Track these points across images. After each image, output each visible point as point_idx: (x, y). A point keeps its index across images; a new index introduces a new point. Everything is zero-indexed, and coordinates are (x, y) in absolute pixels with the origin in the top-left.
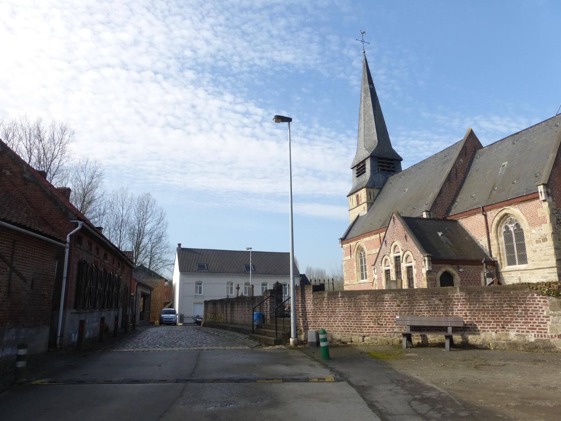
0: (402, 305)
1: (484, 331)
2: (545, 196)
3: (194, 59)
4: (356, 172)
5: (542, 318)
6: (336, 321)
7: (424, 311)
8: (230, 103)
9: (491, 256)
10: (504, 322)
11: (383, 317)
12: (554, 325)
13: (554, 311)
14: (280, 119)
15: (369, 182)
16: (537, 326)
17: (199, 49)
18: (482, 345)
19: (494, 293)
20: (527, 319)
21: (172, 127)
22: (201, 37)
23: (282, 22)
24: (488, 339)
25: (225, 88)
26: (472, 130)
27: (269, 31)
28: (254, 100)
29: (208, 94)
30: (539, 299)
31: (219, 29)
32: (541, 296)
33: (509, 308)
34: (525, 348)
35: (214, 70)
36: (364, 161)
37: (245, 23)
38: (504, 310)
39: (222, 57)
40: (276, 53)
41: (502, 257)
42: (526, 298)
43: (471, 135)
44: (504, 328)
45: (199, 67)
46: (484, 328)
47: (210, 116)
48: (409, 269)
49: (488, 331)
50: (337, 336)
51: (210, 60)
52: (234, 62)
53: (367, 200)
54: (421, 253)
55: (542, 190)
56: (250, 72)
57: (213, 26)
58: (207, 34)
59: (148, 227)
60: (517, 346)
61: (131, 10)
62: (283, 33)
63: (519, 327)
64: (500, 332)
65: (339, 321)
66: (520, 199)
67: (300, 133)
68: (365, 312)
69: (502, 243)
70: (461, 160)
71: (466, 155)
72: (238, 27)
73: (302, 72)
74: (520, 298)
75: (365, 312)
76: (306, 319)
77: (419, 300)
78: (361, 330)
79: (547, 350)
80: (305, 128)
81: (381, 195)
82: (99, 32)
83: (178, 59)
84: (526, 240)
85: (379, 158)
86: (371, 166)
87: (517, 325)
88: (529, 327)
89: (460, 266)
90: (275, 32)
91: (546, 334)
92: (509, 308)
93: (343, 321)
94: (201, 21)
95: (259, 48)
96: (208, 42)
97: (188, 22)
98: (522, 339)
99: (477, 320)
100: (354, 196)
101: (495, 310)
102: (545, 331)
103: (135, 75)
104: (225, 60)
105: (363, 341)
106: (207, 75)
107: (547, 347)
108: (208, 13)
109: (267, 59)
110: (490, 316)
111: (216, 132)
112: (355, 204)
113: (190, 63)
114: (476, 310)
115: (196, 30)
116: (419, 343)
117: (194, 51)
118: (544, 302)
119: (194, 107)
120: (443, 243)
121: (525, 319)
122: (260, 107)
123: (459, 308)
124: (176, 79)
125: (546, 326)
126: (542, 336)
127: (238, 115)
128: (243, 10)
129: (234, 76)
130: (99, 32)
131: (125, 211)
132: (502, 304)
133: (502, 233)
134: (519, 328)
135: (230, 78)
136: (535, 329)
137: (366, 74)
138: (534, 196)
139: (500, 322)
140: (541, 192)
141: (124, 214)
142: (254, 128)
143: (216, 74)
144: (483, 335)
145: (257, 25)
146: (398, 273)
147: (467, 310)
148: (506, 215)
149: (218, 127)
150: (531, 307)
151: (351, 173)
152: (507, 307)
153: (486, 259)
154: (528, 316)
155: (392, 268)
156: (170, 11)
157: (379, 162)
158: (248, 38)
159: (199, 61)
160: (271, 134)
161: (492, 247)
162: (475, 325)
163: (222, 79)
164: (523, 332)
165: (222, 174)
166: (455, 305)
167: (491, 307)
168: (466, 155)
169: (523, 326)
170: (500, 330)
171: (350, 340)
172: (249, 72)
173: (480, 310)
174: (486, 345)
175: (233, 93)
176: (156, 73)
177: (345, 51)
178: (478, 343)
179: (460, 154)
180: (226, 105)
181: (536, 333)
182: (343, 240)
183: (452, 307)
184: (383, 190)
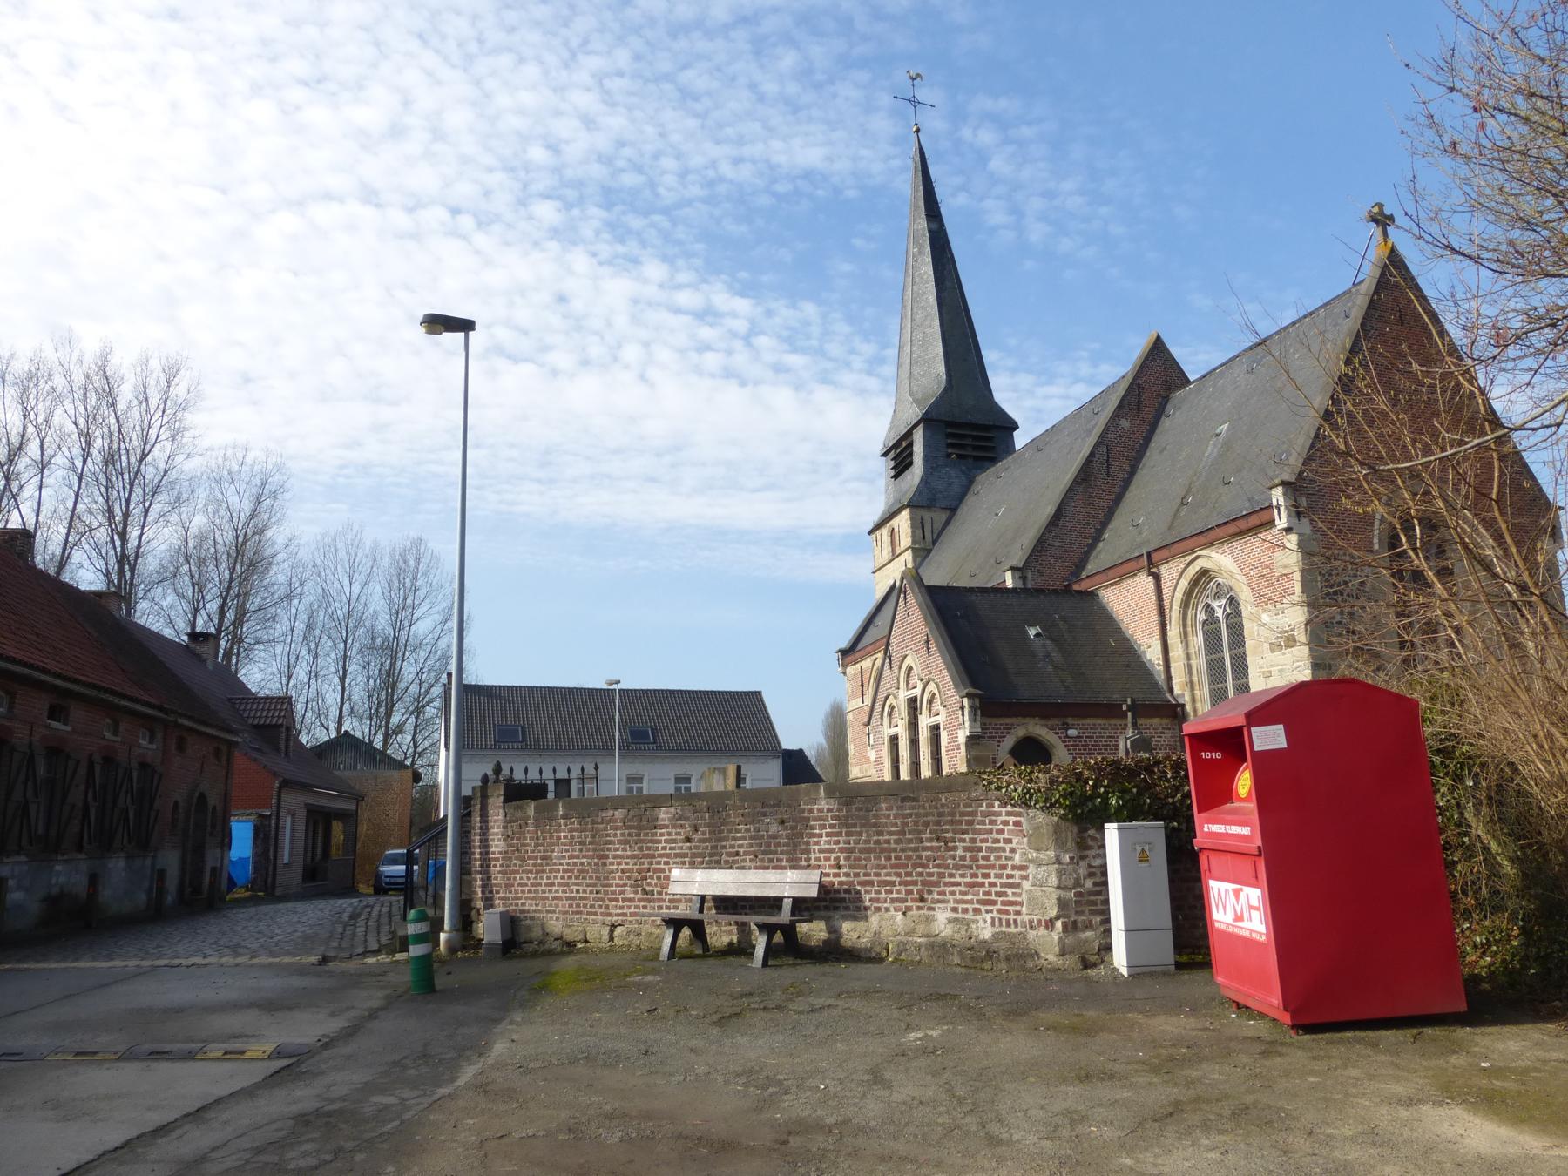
0: (696, 837)
1: (878, 909)
2: (1289, 516)
3: (557, 170)
4: (892, 464)
5: (1009, 871)
6: (553, 884)
7: (746, 854)
8: (661, 286)
9: (1171, 690)
10: (924, 883)
11: (656, 871)
12: (1038, 892)
13: (1038, 850)
14: (438, 323)
15: (919, 491)
16: (999, 894)
17: (567, 142)
18: (870, 950)
19: (903, 800)
20: (975, 875)
21: (509, 357)
22: (570, 107)
23: (788, 60)
24: (886, 934)
25: (644, 244)
26: (1158, 337)
27: (753, 86)
28: (723, 277)
29: (600, 264)
30: (1004, 818)
31: (615, 84)
32: (1009, 808)
33: (935, 844)
34: (963, 958)
35: (609, 197)
36: (909, 434)
37: (686, 66)
38: (925, 849)
39: (630, 160)
40: (776, 144)
41: (1197, 692)
42: (973, 814)
43: (1158, 349)
44: (922, 900)
45: (569, 192)
46: (878, 900)
47: (609, 324)
48: (935, 729)
49: (887, 910)
50: (556, 926)
51: (597, 171)
52: (664, 172)
53: (914, 542)
54: (956, 686)
55: (1282, 502)
56: (710, 201)
57: (600, 78)
58: (585, 100)
59: (422, 628)
60: (947, 951)
61: (377, 44)
62: (792, 88)
63: (958, 897)
64: (914, 912)
65: (560, 884)
66: (1232, 528)
67: (857, 362)
68: (615, 857)
69: (1197, 654)
70: (1125, 424)
71: (1139, 409)
72: (667, 77)
73: (851, 193)
74: (963, 814)
75: (615, 857)
76: (489, 879)
77: (733, 823)
78: (607, 907)
79: (1015, 963)
80: (868, 349)
81: (951, 527)
82: (298, 108)
83: (512, 170)
84: (1249, 644)
85: (950, 424)
86: (925, 446)
87: (953, 893)
88: (981, 897)
89: (1070, 721)
90: (770, 88)
91: (1019, 918)
92: (935, 844)
93: (567, 884)
94: (566, 66)
95: (729, 131)
96: (589, 122)
97: (532, 71)
98: (963, 932)
99: (862, 878)
100: (884, 533)
101: (903, 850)
102: (1017, 908)
103: (401, 220)
104: (639, 169)
105: (611, 939)
106: (594, 211)
107: (1018, 956)
108: (585, 42)
109: (754, 162)
110: (893, 867)
111: (627, 367)
112: (887, 555)
113: (543, 183)
114: (861, 851)
115: (555, 90)
116: (731, 944)
117: (554, 148)
118: (1017, 824)
119: (562, 299)
120: (1034, 656)
121: (972, 876)
122: (742, 294)
123: (823, 846)
124: (509, 226)
125: (1020, 895)
126: (1008, 925)
127: (686, 319)
128: (678, 30)
129: (665, 211)
130: (298, 108)
131: (356, 588)
132: (920, 832)
133: (1199, 626)
134: (957, 901)
135: (657, 218)
136: (993, 903)
137: (921, 194)
138: (1254, 522)
139: (915, 883)
140: (1278, 507)
141: (354, 597)
142: (730, 352)
143: (620, 207)
144: (874, 920)
145: (719, 69)
146: (914, 743)
147: (842, 850)
148: (1204, 572)
149: (631, 353)
150: (986, 841)
151: (884, 467)
152: (931, 840)
153: (1133, 700)
154: (978, 867)
155: (901, 730)
156: (481, 41)
157: (949, 435)
158: (698, 107)
159: (569, 173)
160: (778, 369)
161: (1173, 665)
162: (858, 892)
163: (636, 223)
164: (965, 911)
165: (653, 480)
166: (814, 835)
167: (896, 842)
168: (1139, 409)
169: (966, 893)
170: (914, 905)
171: (581, 937)
172: (706, 201)
173: (869, 851)
174: (878, 949)
175: (665, 258)
176: (455, 211)
177: (966, 133)
178: (864, 942)
179: (1120, 406)
180: (651, 291)
181: (995, 914)
182: (848, 654)
183: (808, 843)
184: (959, 511)
